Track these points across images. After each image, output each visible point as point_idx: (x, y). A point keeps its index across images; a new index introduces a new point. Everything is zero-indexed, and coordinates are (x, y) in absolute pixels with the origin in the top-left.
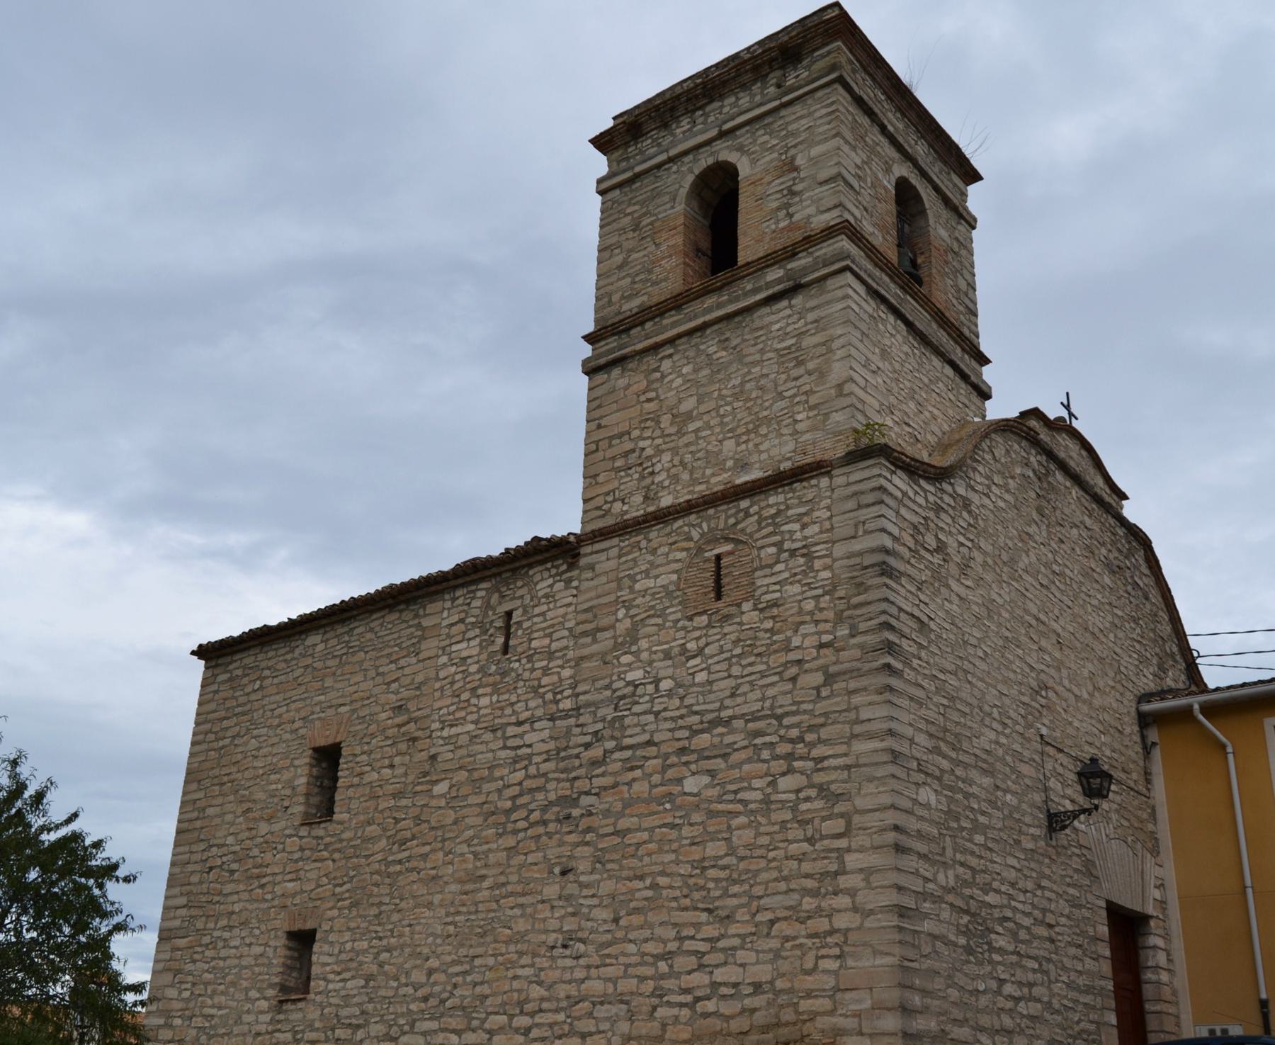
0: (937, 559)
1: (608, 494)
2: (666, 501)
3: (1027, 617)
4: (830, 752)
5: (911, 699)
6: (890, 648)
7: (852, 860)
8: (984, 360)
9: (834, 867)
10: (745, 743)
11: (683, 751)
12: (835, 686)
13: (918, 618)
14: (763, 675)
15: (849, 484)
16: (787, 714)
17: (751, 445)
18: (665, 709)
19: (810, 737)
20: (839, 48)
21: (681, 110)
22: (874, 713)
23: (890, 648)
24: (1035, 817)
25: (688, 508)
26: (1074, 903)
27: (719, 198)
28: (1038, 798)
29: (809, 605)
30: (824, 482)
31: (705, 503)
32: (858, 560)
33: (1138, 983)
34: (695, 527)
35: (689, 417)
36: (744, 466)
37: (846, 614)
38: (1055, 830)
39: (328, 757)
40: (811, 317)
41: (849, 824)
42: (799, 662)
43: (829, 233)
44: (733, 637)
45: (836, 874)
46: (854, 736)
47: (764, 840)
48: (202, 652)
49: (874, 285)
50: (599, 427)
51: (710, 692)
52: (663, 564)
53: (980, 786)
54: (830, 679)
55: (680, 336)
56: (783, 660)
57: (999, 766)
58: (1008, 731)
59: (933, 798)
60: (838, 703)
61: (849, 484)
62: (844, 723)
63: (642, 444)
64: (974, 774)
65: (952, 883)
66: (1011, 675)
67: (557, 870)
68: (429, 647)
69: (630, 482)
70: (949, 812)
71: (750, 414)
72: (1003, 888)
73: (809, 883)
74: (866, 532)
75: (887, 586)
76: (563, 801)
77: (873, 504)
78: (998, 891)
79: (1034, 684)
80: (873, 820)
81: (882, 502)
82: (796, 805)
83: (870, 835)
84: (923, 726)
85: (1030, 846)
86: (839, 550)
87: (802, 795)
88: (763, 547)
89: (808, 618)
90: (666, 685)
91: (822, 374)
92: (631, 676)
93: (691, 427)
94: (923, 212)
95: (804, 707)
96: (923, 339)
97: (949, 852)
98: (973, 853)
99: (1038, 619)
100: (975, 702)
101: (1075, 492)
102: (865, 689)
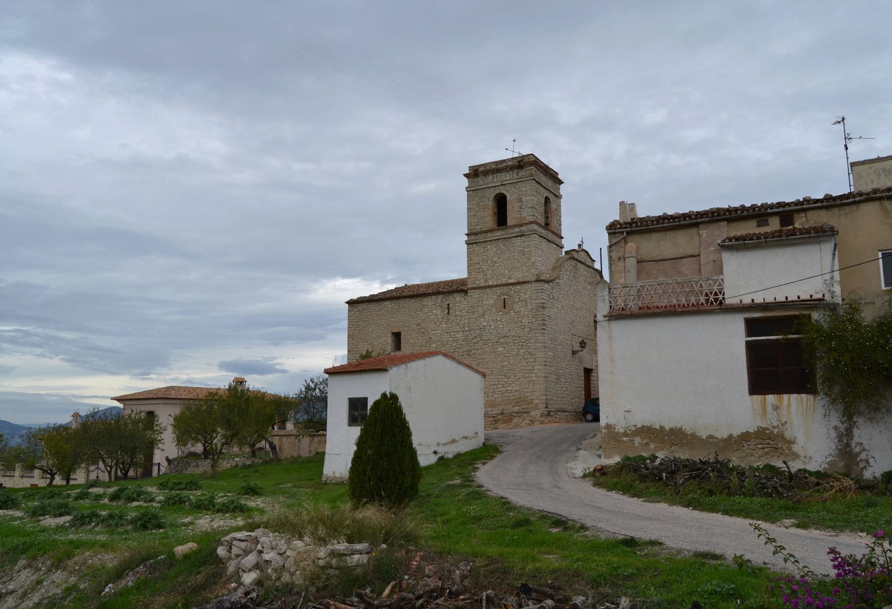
2: (491, 283)
6: (544, 324)
7: (536, 367)
22: (541, 338)
23: (544, 324)
25: (497, 286)
26: (577, 369)
27: (501, 202)
33: (589, 384)
34: (499, 291)
36: (510, 278)
39: (397, 336)
48: (347, 303)
52: (490, 299)
54: (531, 330)
68: (426, 310)
69: (480, 276)
76: (467, 351)
80: (540, 360)
86: (533, 302)
91: (529, 259)
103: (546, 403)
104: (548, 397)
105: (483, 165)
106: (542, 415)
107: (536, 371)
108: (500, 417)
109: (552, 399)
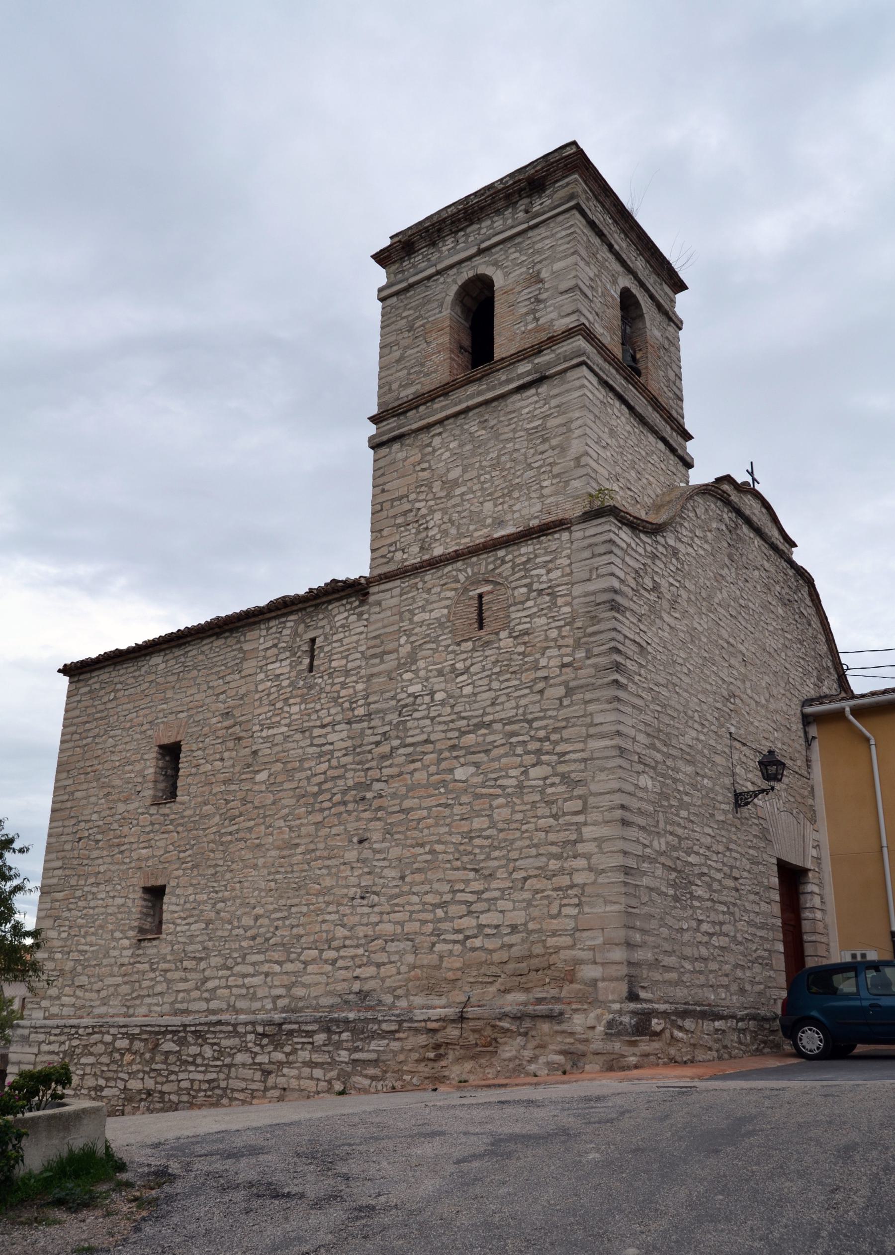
0: (653, 597)
1: (391, 545)
2: (438, 551)
3: (720, 642)
4: (571, 749)
5: (634, 707)
6: (618, 667)
7: (588, 832)
8: (688, 437)
9: (573, 837)
10: (503, 741)
11: (453, 747)
12: (574, 697)
13: (638, 643)
14: (517, 688)
15: (585, 538)
16: (536, 719)
17: (506, 506)
18: (439, 715)
19: (554, 737)
20: (576, 180)
21: (447, 231)
22: (605, 718)
23: (618, 667)
24: (725, 796)
25: (457, 556)
26: (754, 862)
27: (478, 305)
28: (728, 781)
29: (554, 634)
30: (565, 536)
31: (470, 553)
32: (592, 598)
34: (461, 572)
35: (455, 483)
36: (501, 523)
37: (583, 640)
38: (740, 806)
39: (171, 753)
40: (554, 403)
41: (585, 803)
42: (546, 678)
43: (569, 333)
44: (493, 659)
45: (575, 842)
46: (589, 736)
47: (519, 816)
48: (66, 670)
49: (605, 377)
50: (383, 491)
51: (475, 702)
52: (436, 601)
53: (685, 773)
55: (447, 418)
56: (533, 676)
57: (698, 757)
58: (705, 730)
59: (650, 784)
60: (577, 710)
61: (585, 538)
62: (581, 726)
63: (417, 505)
64: (680, 764)
65: (664, 848)
66: (708, 687)
67: (355, 840)
68: (249, 666)
69: (409, 536)
70: (661, 794)
71: (505, 481)
72: (701, 851)
73: (554, 849)
74: (599, 576)
75: (616, 619)
76: (359, 786)
77: (605, 554)
78: (697, 853)
79: (725, 693)
81: (611, 552)
82: (544, 790)
83: (602, 812)
84: (642, 727)
85: (722, 818)
86: (577, 590)
87: (548, 782)
88: (516, 588)
89: (552, 644)
90: (439, 696)
91: (562, 449)
92: (411, 690)
93: (458, 491)
94: (642, 316)
95: (549, 713)
96: (642, 420)
97: (662, 825)
98: (679, 825)
99: (728, 643)
100: (681, 708)
101: (757, 541)
102: (598, 700)
103: (632, 980)
104: (640, 955)
105: (427, 218)
106: (613, 1030)
107: (590, 847)
108: (453, 1032)
109: (656, 964)
